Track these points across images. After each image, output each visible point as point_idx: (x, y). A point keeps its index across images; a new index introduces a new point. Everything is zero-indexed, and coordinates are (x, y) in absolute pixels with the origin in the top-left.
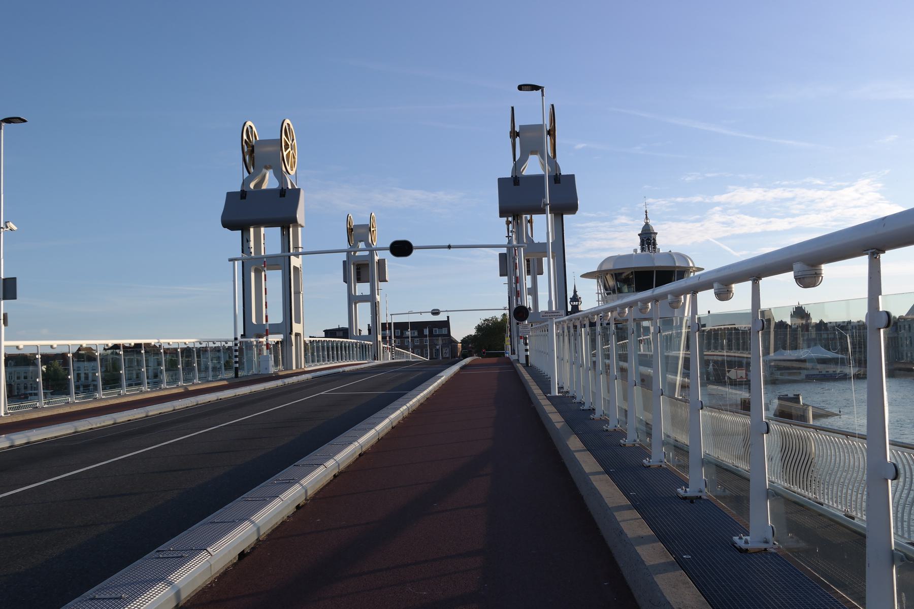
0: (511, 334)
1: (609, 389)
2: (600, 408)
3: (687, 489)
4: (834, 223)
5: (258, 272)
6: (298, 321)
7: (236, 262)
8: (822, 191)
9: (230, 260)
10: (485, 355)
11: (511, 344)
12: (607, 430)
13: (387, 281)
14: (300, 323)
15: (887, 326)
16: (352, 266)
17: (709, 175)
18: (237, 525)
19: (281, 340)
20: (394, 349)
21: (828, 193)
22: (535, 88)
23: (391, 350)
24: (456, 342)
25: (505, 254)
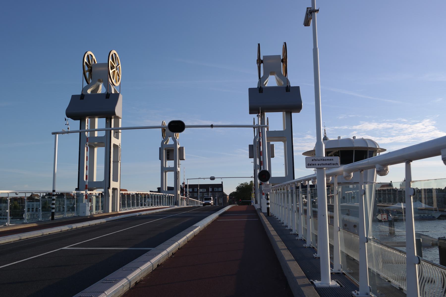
0: (255, 191)
1: (306, 222)
2: (310, 241)
4: (413, 140)
5: (92, 148)
6: (115, 180)
7: (57, 135)
8: (406, 125)
9: (53, 133)
10: (241, 202)
11: (255, 197)
13: (184, 160)
14: (117, 181)
16: (164, 150)
17: (350, 116)
18: (190, 232)
19: (101, 192)
20: (189, 199)
21: (409, 125)
23: (187, 200)
24: (226, 195)
25: (253, 145)
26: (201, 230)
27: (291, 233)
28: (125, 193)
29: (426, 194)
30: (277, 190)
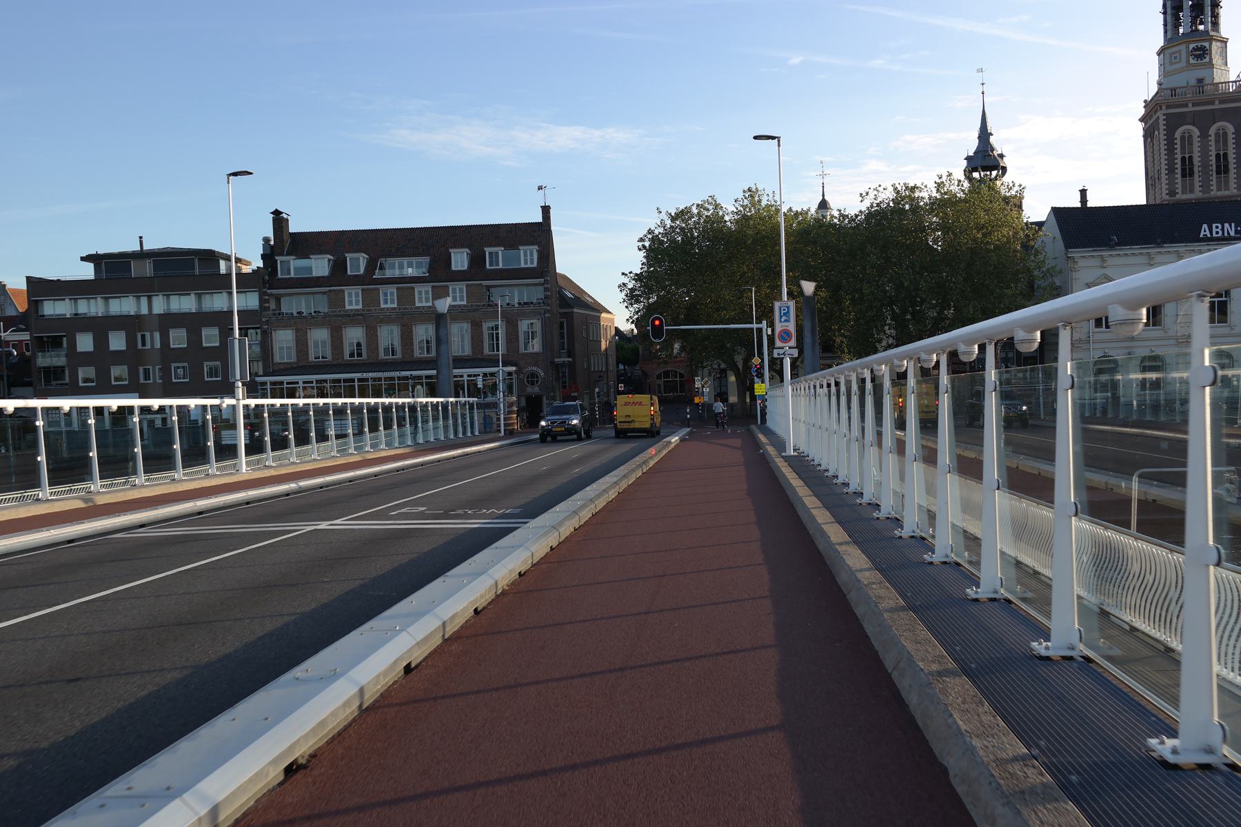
2: (912, 523)
3: (979, 590)
12: (901, 537)
15: (1213, 384)
22: (773, 138)
26: (369, 699)
27: (860, 502)
28: (405, 403)
29: (240, 402)
30: (818, 386)
